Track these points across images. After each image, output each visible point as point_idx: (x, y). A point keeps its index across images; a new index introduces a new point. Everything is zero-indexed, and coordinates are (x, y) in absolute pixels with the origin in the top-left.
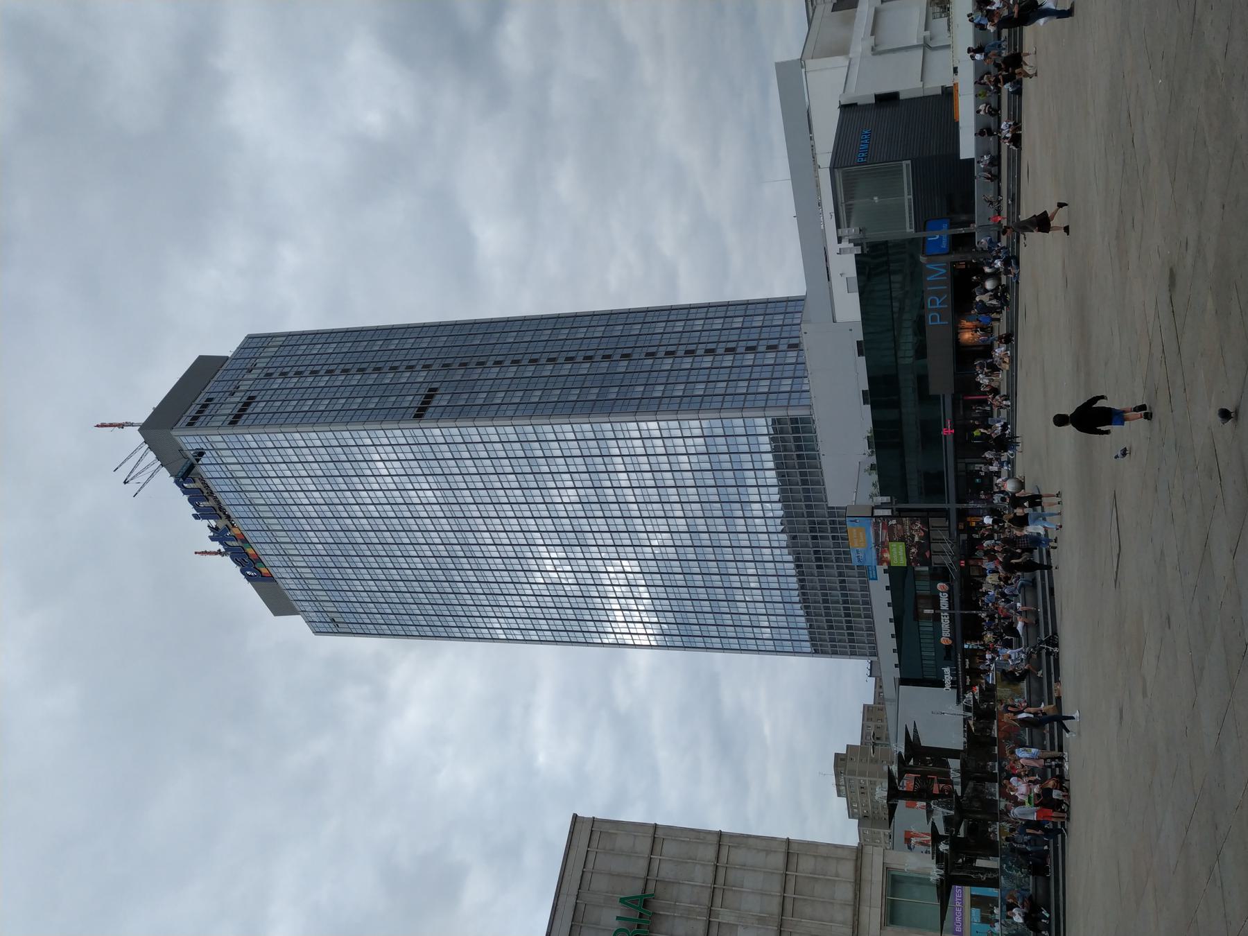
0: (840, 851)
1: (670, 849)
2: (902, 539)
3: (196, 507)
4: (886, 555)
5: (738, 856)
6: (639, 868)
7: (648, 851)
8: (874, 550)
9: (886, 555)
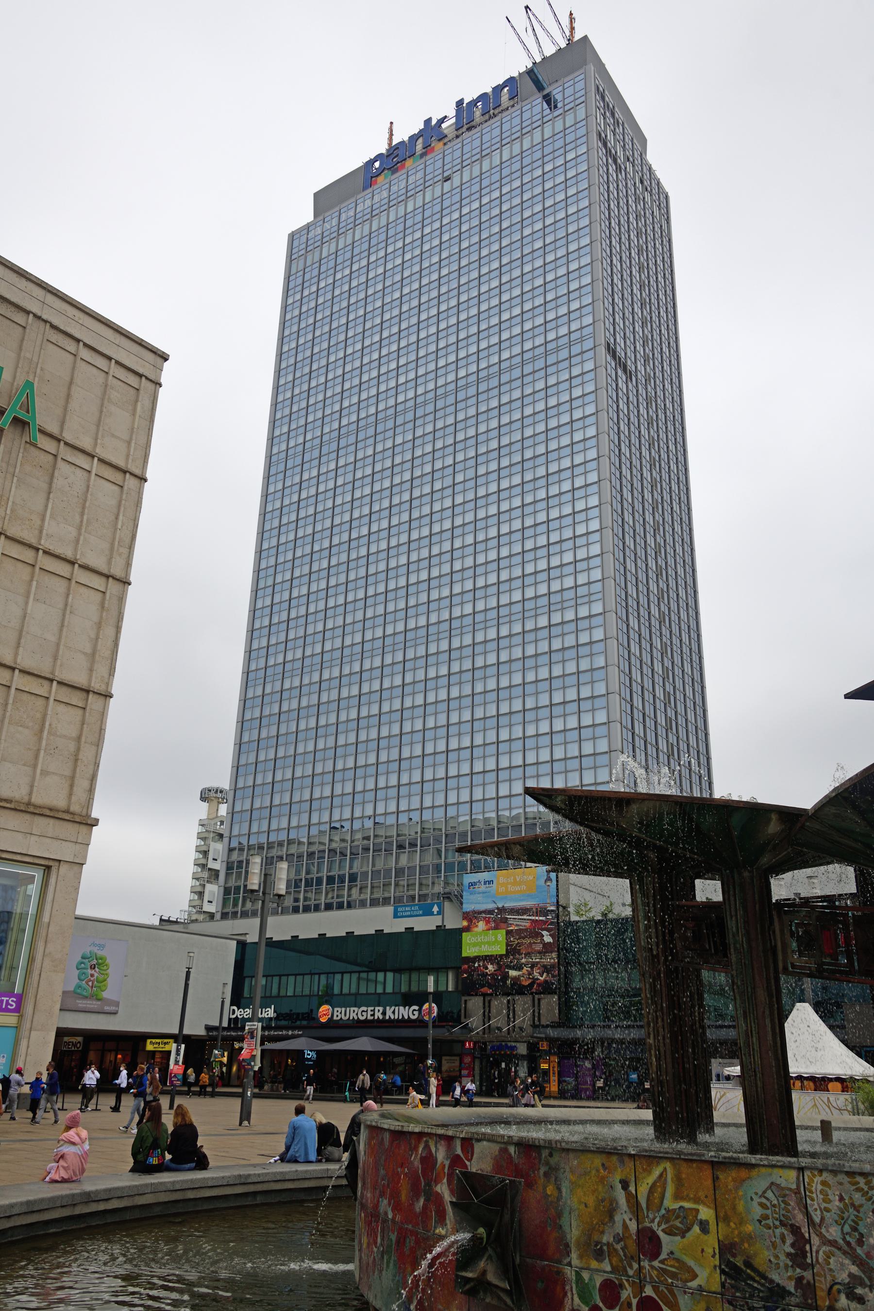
0: (86, 784)
1: (104, 493)
2: (512, 950)
3: (473, 103)
4: (481, 925)
5: (86, 604)
6: (77, 432)
7: (104, 456)
8: (491, 906)
9: (481, 925)
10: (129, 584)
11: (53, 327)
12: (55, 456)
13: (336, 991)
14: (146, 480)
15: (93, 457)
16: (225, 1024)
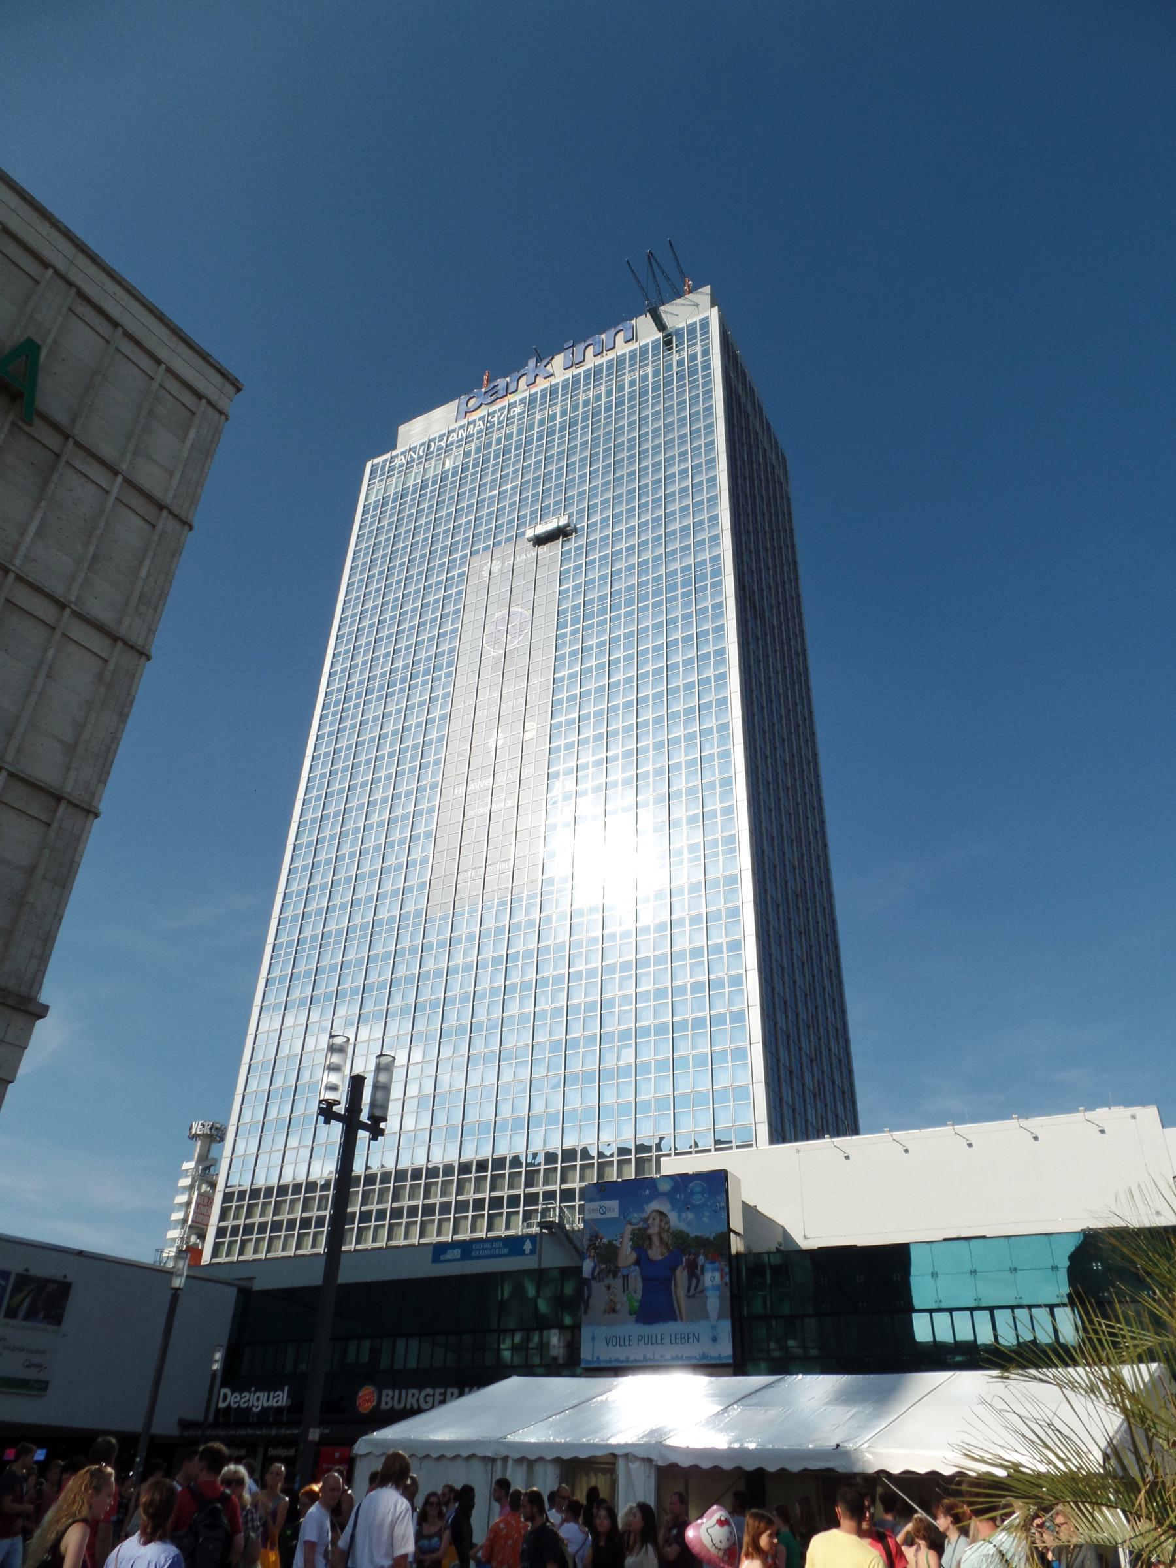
1: (129, 529)
6: (99, 433)
10: (97, 815)
11: (81, 295)
12: (58, 456)
13: (384, 1365)
14: (148, 658)
15: (116, 473)
16: (211, 1418)
